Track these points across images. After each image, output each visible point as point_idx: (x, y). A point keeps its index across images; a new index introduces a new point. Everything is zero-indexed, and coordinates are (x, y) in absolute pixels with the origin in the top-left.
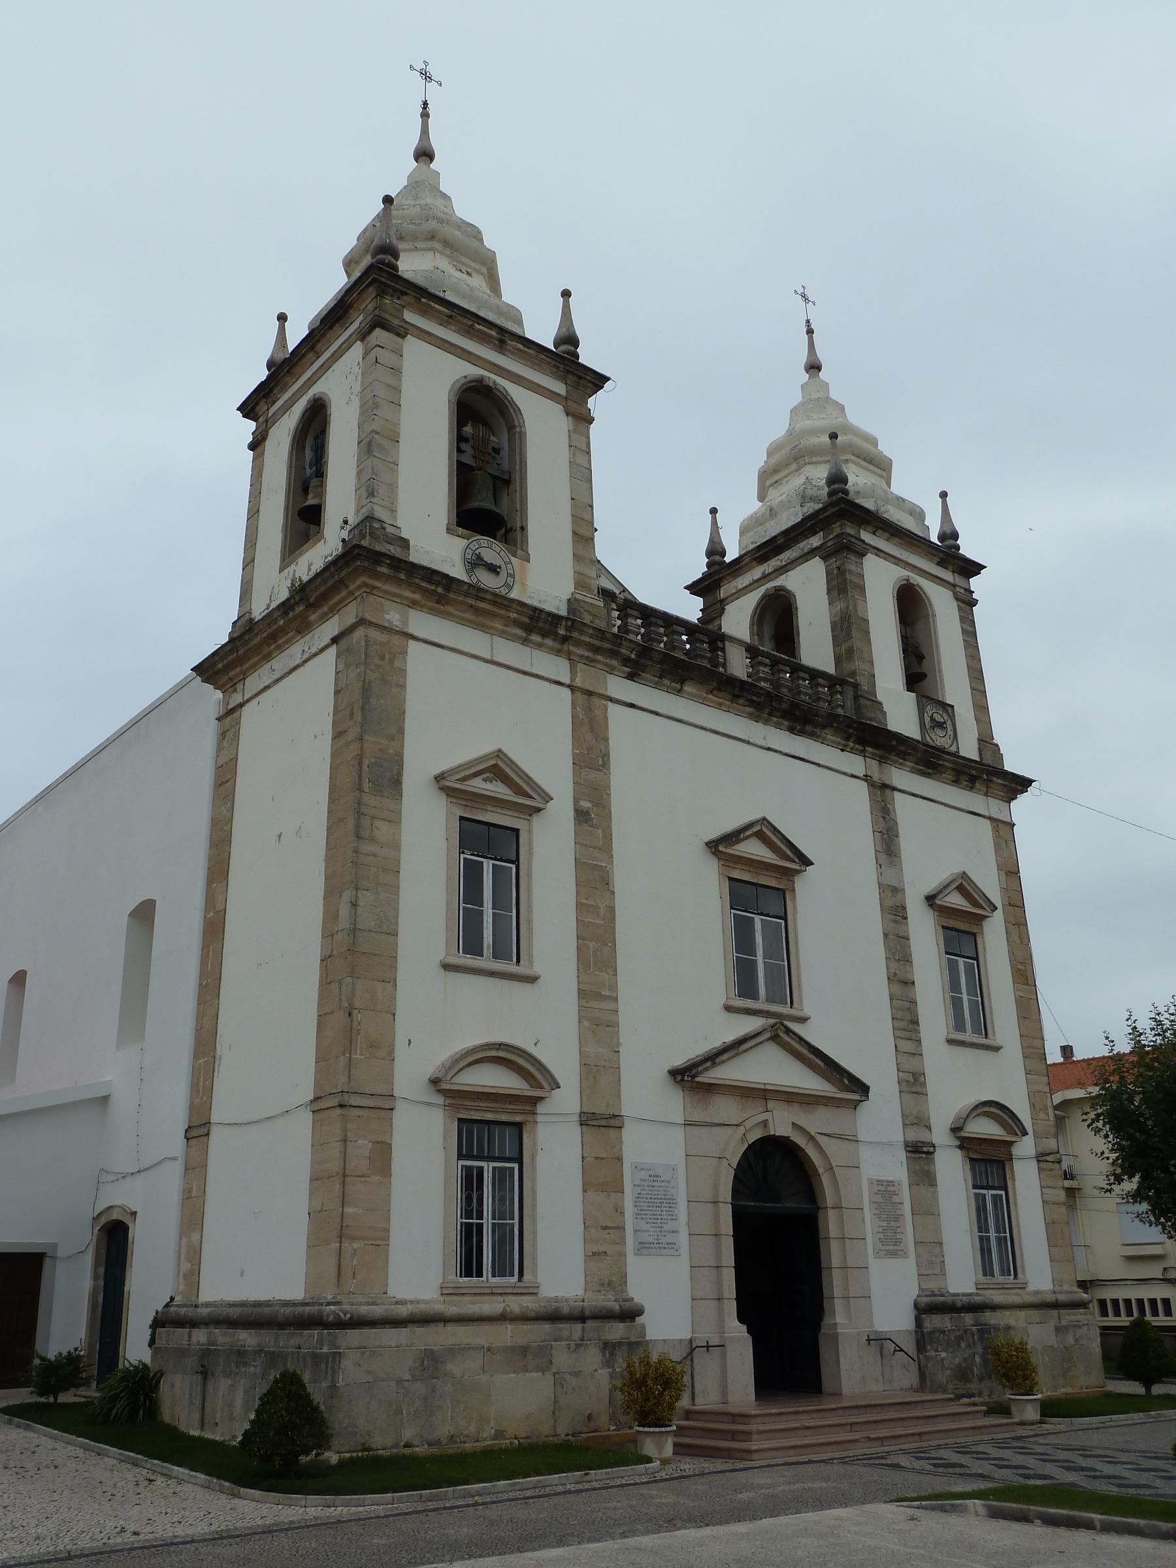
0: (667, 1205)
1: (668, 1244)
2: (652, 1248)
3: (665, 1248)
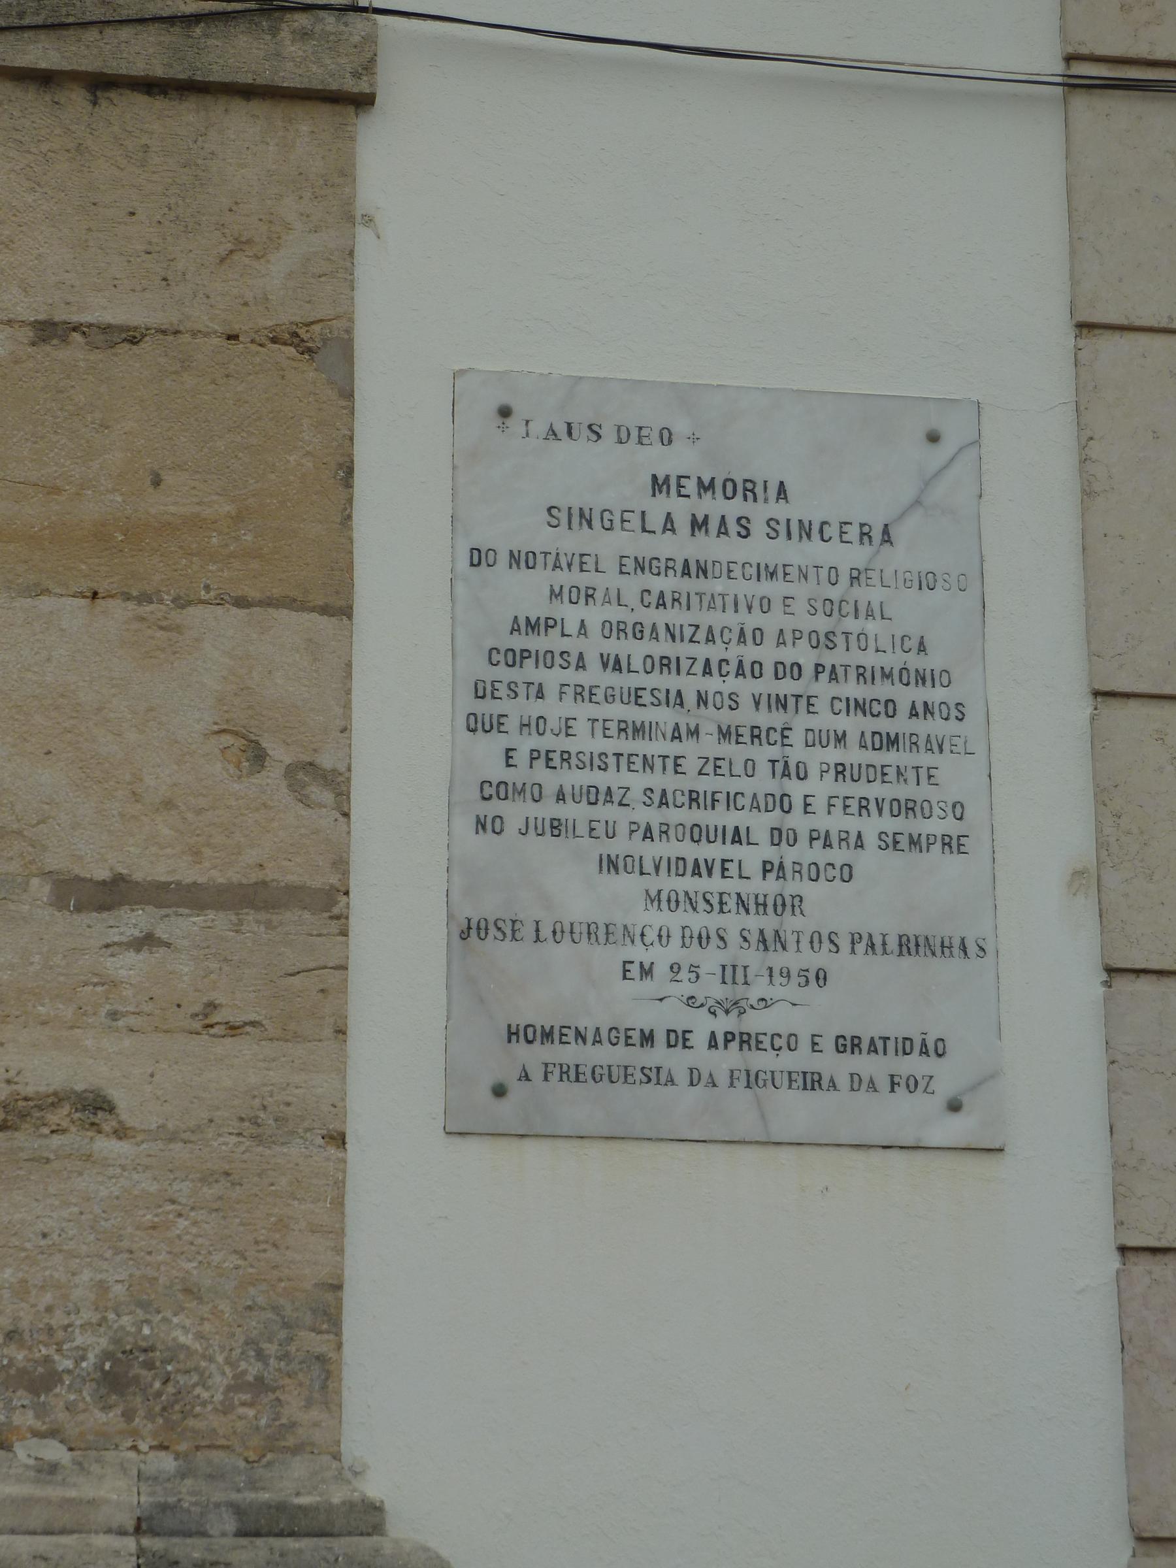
0: (853, 724)
1: (849, 1045)
2: (653, 1076)
3: (812, 1082)
